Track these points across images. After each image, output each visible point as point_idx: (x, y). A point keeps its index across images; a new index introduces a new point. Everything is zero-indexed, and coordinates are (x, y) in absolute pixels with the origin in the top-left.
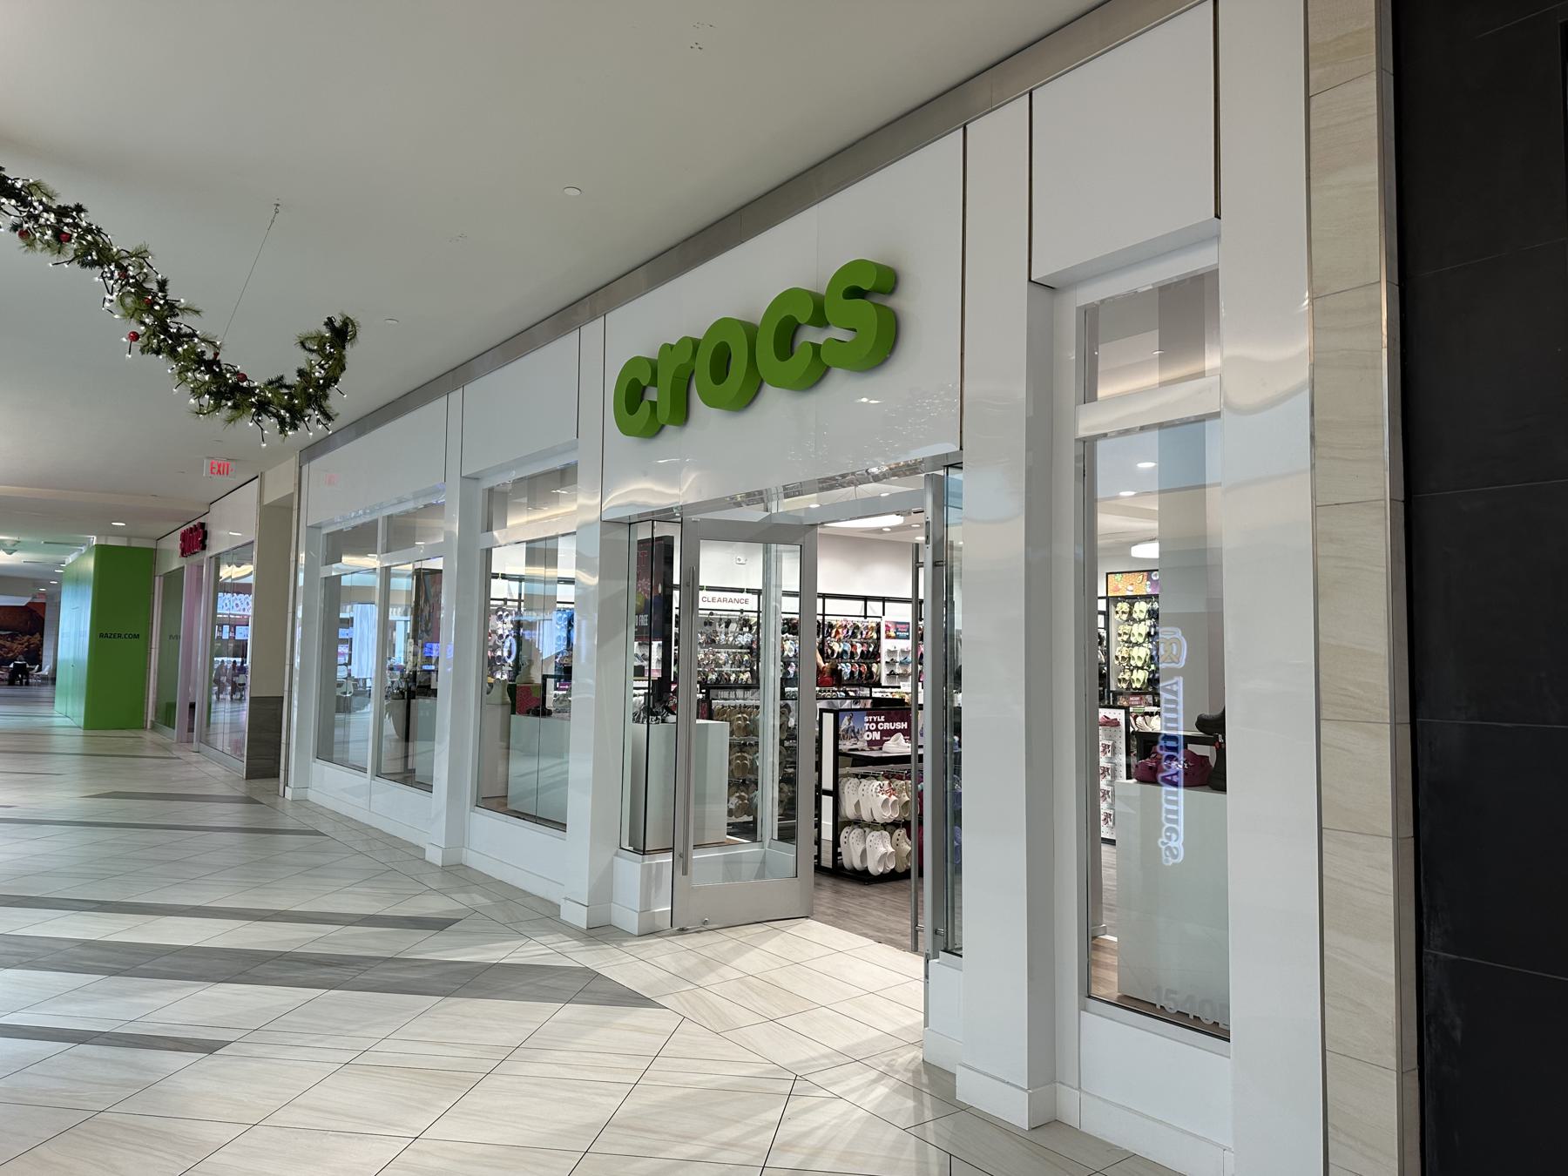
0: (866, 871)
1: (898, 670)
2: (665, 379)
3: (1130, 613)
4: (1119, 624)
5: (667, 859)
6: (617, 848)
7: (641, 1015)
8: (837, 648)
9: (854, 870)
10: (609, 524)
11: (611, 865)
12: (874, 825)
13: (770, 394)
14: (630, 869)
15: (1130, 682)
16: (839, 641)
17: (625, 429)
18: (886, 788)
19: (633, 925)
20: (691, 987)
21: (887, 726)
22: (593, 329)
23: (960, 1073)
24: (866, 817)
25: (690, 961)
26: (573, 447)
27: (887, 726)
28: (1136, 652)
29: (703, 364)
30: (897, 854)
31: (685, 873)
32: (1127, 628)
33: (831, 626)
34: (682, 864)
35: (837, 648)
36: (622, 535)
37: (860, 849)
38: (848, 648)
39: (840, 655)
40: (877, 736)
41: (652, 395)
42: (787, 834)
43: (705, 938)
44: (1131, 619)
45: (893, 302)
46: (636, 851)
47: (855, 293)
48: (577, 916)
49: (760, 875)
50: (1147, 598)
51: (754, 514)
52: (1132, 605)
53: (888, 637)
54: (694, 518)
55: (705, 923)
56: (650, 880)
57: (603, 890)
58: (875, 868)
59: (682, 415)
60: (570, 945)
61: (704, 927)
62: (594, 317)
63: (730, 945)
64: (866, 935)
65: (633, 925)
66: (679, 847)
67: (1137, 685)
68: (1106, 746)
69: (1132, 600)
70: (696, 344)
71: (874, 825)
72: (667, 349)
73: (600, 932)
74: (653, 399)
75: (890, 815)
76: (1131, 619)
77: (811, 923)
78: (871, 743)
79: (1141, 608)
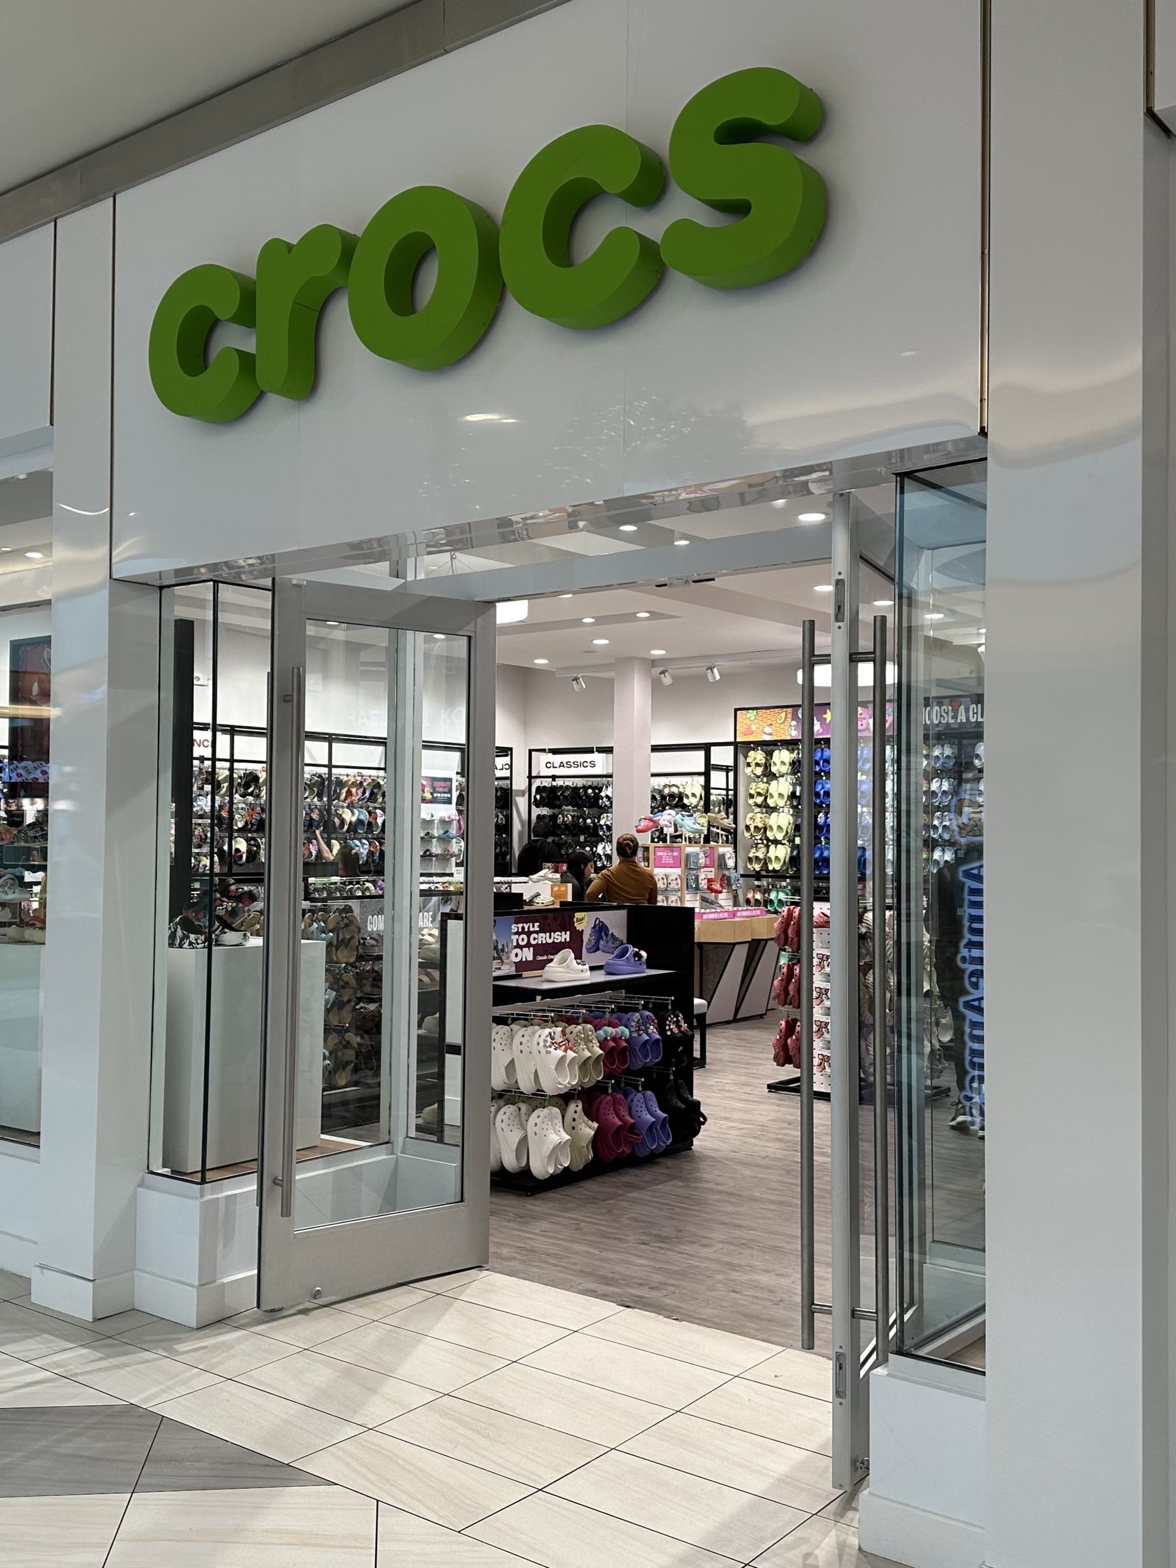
0: (526, 1172)
1: (436, 849)
2: (275, 309)
3: (767, 766)
4: (750, 780)
5: (248, 1186)
6: (141, 1173)
7: (288, 1507)
8: (348, 816)
9: (552, 1176)
10: (125, 586)
11: (134, 1199)
12: (538, 1099)
13: (519, 329)
14: (175, 1211)
15: (766, 861)
16: (351, 807)
17: (172, 398)
18: (559, 1039)
19: (184, 1306)
20: (351, 1431)
21: (543, 938)
22: (86, 226)
23: (36, 1277)
24: (526, 1085)
25: (321, 1375)
26: (40, 441)
27: (543, 938)
28: (774, 820)
29: (371, 270)
30: (573, 1144)
31: (286, 1211)
32: (762, 787)
33: (340, 784)
34: (276, 1192)
35: (348, 816)
36: (145, 608)
37: (515, 1137)
38: (365, 816)
39: (353, 827)
40: (528, 954)
41: (233, 339)
42: (433, 1129)
43: (321, 1325)
44: (769, 775)
45: (819, 156)
46: (178, 1174)
47: (739, 132)
48: (79, 1302)
49: (390, 1201)
50: (790, 744)
51: (375, 576)
52: (769, 754)
53: (424, 800)
54: (296, 578)
55: (317, 1294)
56: (215, 1227)
57: (118, 1252)
58: (541, 1167)
59: (305, 377)
60: (75, 1357)
61: (316, 1301)
62: (89, 199)
63: (374, 1334)
64: (604, 1297)
65: (184, 1306)
66: (274, 1166)
67: (775, 866)
68: (823, 958)
69: (769, 747)
70: (348, 246)
71: (538, 1099)
72: (275, 251)
73: (120, 1325)
74: (229, 348)
75: (568, 1080)
76: (769, 775)
77: (488, 1278)
78: (522, 966)
79: (782, 758)
